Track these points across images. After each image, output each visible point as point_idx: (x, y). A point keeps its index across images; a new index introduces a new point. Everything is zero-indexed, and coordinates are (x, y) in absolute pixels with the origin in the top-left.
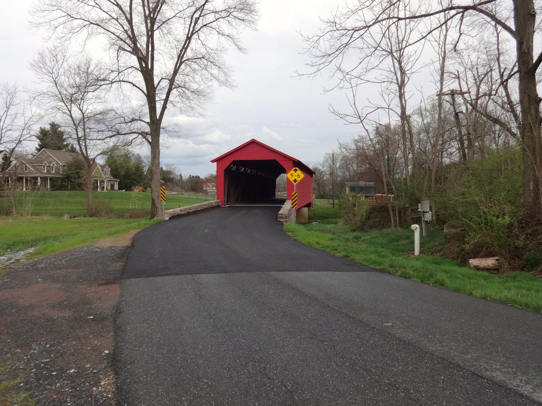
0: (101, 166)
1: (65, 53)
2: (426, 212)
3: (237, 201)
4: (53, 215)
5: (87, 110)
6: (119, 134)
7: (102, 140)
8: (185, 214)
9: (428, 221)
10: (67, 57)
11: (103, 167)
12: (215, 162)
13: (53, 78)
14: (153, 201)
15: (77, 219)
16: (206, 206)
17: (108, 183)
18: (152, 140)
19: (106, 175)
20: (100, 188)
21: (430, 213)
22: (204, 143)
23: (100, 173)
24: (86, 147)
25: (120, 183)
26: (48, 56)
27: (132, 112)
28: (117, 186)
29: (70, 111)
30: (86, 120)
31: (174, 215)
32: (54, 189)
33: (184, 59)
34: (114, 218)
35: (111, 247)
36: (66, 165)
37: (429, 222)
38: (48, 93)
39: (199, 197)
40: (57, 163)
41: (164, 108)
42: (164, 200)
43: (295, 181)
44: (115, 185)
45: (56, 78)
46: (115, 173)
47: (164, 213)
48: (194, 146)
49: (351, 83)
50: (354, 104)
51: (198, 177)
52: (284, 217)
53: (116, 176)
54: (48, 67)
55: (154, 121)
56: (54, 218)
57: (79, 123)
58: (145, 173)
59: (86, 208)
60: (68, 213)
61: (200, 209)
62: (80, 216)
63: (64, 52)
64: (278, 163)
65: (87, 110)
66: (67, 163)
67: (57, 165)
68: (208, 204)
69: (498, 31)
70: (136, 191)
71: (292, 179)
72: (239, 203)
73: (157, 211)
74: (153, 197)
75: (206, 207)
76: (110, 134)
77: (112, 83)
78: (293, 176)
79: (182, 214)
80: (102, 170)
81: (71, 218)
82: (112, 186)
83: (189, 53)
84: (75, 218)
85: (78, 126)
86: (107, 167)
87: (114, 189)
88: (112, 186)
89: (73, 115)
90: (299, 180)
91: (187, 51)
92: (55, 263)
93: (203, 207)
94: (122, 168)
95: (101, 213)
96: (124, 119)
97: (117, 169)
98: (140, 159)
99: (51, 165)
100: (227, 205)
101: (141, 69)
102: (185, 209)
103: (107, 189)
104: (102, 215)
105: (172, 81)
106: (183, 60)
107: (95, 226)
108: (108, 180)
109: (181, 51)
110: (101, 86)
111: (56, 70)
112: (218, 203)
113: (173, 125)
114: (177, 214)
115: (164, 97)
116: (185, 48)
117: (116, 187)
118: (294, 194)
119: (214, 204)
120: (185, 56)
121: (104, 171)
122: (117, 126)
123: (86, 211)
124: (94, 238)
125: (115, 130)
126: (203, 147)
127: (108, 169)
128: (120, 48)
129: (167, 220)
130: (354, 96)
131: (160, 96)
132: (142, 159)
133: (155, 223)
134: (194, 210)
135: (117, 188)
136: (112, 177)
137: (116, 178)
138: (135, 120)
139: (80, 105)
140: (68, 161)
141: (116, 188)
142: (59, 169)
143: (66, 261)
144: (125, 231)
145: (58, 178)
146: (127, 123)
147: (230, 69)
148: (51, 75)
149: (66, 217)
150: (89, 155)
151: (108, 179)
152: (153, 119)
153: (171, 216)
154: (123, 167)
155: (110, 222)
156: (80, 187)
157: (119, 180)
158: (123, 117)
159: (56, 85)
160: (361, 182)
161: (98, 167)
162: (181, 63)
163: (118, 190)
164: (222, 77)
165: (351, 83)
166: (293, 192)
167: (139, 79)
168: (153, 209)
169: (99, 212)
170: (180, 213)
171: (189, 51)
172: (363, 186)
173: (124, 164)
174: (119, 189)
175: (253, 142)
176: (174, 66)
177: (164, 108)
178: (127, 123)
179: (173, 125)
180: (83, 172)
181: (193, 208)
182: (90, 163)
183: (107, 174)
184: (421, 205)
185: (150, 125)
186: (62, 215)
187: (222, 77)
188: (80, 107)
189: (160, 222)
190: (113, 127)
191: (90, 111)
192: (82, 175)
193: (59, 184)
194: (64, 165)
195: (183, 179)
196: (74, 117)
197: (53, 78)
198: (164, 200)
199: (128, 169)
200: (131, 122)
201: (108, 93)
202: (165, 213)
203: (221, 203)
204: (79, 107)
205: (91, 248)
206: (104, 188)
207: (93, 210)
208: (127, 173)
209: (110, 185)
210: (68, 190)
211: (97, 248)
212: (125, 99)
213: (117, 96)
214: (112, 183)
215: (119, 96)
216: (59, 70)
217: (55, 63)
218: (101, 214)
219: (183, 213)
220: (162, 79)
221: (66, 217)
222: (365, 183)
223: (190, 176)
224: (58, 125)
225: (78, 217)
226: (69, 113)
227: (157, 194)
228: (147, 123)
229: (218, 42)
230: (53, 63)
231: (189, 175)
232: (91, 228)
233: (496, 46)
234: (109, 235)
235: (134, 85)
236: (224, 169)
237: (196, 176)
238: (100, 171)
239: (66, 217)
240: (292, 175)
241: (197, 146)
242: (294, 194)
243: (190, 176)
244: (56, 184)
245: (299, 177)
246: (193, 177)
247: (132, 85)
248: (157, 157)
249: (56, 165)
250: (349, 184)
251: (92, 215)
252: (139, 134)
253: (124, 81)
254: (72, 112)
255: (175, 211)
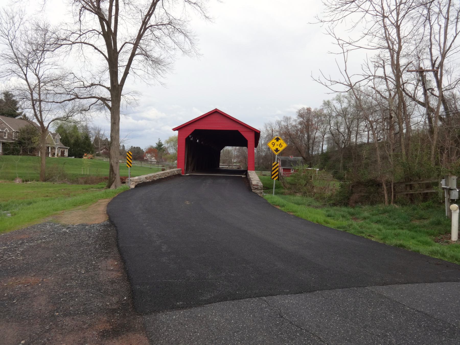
0: (52, 134)
1: (23, 16)
2: (452, 190)
3: (193, 170)
4: (5, 179)
5: (42, 75)
6: (77, 97)
7: (60, 103)
8: (149, 182)
9: (455, 200)
10: (24, 20)
11: (54, 135)
12: (176, 130)
13: (9, 40)
14: (111, 167)
15: (30, 184)
16: (169, 174)
17: (59, 150)
18: (112, 105)
19: (57, 144)
20: (51, 154)
21: (458, 190)
22: (142, 119)
23: (52, 140)
24: (41, 112)
25: (70, 151)
26: (4, 17)
27: (91, 76)
28: (67, 153)
29: (26, 75)
30: (42, 84)
31: (140, 183)
32: (7, 152)
33: (149, 26)
34: (68, 183)
35: (82, 225)
36: (19, 131)
37: (455, 200)
38: (3, 55)
39: (143, 166)
40: (10, 129)
41: (126, 73)
42: (130, 167)
43: (277, 150)
44: (65, 152)
45: (12, 41)
46: (65, 141)
47: (129, 181)
48: (134, 121)
49: (343, 48)
50: (346, 71)
51: (138, 148)
52: (259, 188)
53: (66, 143)
54: (4, 29)
55: (115, 86)
56: (5, 182)
57: (34, 88)
58: (92, 143)
59: (39, 172)
60: (20, 177)
61: (163, 177)
62: (33, 180)
63: (21, 15)
64: (240, 133)
65: (42, 75)
66: (20, 130)
67: (10, 131)
68: (170, 172)
69: (431, 24)
70: (86, 158)
71: (273, 148)
72: (196, 172)
73: (115, 178)
74: (111, 163)
75: (169, 175)
76: (68, 97)
77: (74, 43)
78: (274, 145)
79: (148, 182)
80: (53, 138)
81: (23, 181)
82: (63, 153)
83: (152, 21)
84: (27, 183)
85: (33, 91)
86: (58, 135)
87: (64, 155)
88: (63, 153)
89: (28, 79)
90: (281, 149)
91: (150, 19)
92: (5, 257)
93: (166, 176)
94: (71, 137)
95: (54, 177)
96: (84, 83)
97: (67, 137)
98: (87, 130)
99: (4, 131)
100: (187, 173)
101: (103, 33)
102: (150, 177)
103: (57, 155)
104: (56, 179)
105: (136, 45)
106: (147, 26)
107: (50, 191)
108: (59, 148)
109: (146, 16)
110: (62, 45)
111: (13, 32)
112: (179, 172)
113: (132, 93)
114: (143, 182)
115: (126, 63)
116: (149, 15)
117: (66, 154)
118: (276, 165)
119: (176, 172)
120: (149, 23)
121: (55, 139)
122: (76, 90)
123: (38, 175)
124: (56, 210)
125: (74, 94)
126: (141, 123)
127: (58, 137)
128: (83, 7)
129: (132, 189)
130: (345, 62)
131: (123, 60)
132: (89, 130)
133: (122, 191)
134: (158, 178)
135: (67, 155)
136: (62, 145)
137: (66, 146)
138: (95, 85)
139: (36, 70)
140: (21, 128)
141: (66, 155)
142: (12, 135)
143: (23, 253)
144: (92, 200)
145: (11, 143)
146: (86, 87)
147: (196, 38)
148: (7, 37)
149: (18, 181)
150: (43, 120)
151: (59, 146)
152: (115, 84)
153: (137, 184)
154: (72, 137)
155: (65, 188)
156: (32, 151)
157: (69, 148)
158: (82, 81)
159: (12, 47)
160: (291, 157)
161: (50, 134)
162: (145, 29)
163: (67, 157)
164: (187, 46)
165: (343, 48)
166: (273, 163)
167: (101, 43)
168: (111, 176)
169: (52, 177)
170: (145, 181)
171: (153, 17)
172: (293, 160)
173: (73, 134)
174: (69, 156)
175: (216, 112)
176: (138, 31)
177: (126, 73)
178: (86, 87)
179: (132, 93)
180: (36, 139)
181: (158, 176)
182: (44, 130)
183: (58, 141)
184: (446, 181)
185: (110, 91)
186: (13, 179)
187: (187, 46)
188: (36, 72)
189: (127, 191)
190: (73, 91)
191: (46, 77)
192: (34, 141)
193: (12, 147)
194: (16, 132)
195: (125, 150)
196: (29, 82)
197: (9, 40)
198: (130, 167)
199: (77, 137)
200: (90, 86)
201: (67, 56)
202: (130, 180)
203: (181, 171)
204: (34, 71)
205: (56, 226)
206: (54, 154)
207: (47, 175)
208: (77, 142)
209: (60, 152)
210: (21, 155)
211: (64, 226)
212: (86, 62)
213: (78, 58)
214: (62, 150)
215: (80, 58)
216: (15, 32)
217: (11, 25)
218: (54, 179)
219: (148, 181)
220: (126, 43)
221: (18, 181)
222: (294, 157)
223: (132, 147)
224: (11, 94)
225: (31, 181)
226: (24, 77)
227: (115, 160)
228: (108, 88)
229: (184, 10)
230: (9, 25)
231: (131, 147)
232: (47, 194)
233: (429, 37)
234: (74, 206)
235: (96, 48)
236: (185, 138)
237: (137, 147)
238: (51, 138)
239: (18, 181)
240: (273, 144)
241: (136, 122)
242: (276, 165)
243: (132, 147)
244: (9, 148)
245: (281, 146)
246: (134, 147)
247: (94, 48)
248: (117, 123)
249: (9, 131)
250: (280, 158)
251: (45, 180)
252: (99, 99)
253: (86, 43)
254: (27, 76)
255: (140, 179)
